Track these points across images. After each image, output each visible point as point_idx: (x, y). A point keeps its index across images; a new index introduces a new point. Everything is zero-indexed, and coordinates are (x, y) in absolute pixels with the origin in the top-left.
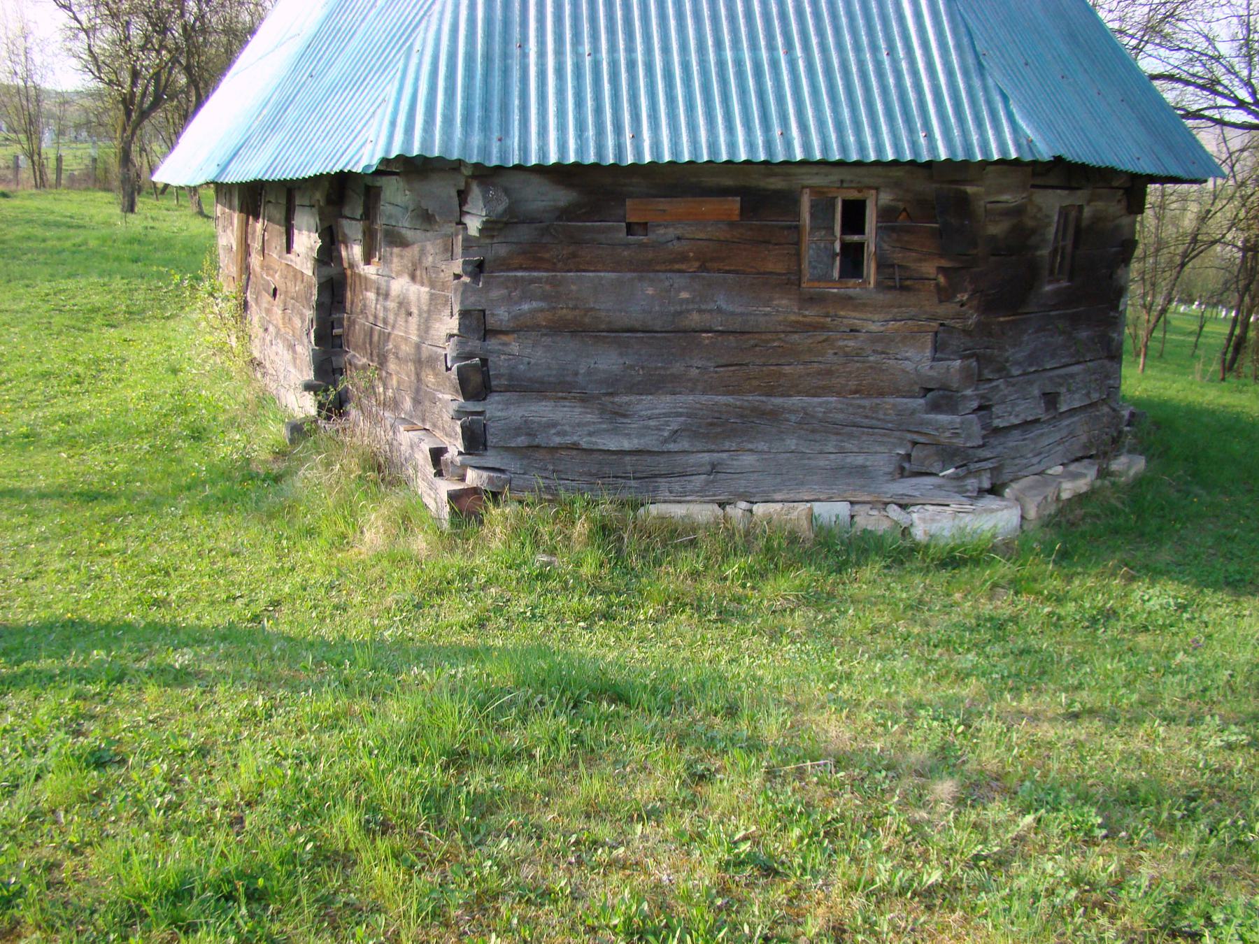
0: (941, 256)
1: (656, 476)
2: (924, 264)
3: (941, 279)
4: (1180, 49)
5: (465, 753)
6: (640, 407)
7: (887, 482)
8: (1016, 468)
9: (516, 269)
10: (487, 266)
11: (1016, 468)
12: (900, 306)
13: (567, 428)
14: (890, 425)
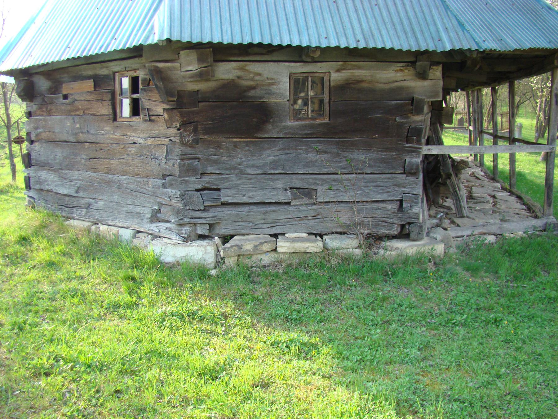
0: (164, 102)
1: (73, 207)
2: (158, 107)
3: (166, 116)
4: (16, 198)
5: (9, 245)
6: (69, 175)
7: (147, 222)
8: (237, 227)
9: (38, 116)
10: (32, 114)
11: (237, 227)
12: (151, 130)
13: (50, 183)
14: (150, 193)
